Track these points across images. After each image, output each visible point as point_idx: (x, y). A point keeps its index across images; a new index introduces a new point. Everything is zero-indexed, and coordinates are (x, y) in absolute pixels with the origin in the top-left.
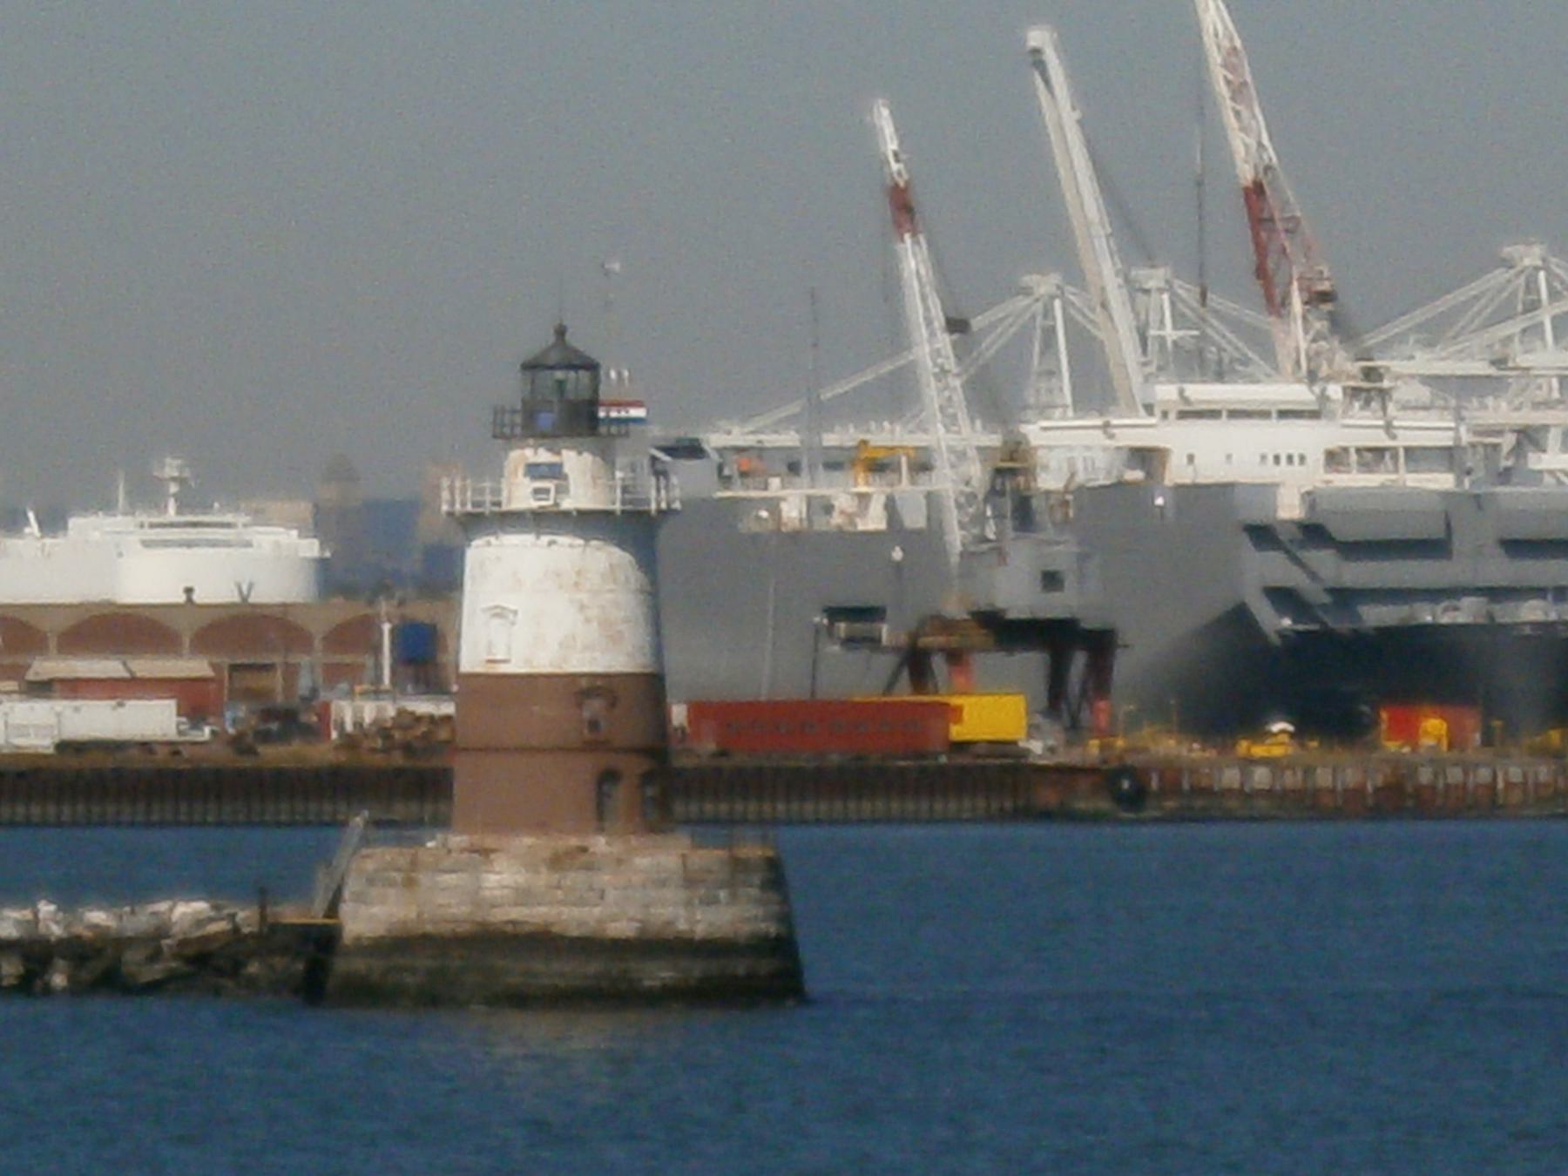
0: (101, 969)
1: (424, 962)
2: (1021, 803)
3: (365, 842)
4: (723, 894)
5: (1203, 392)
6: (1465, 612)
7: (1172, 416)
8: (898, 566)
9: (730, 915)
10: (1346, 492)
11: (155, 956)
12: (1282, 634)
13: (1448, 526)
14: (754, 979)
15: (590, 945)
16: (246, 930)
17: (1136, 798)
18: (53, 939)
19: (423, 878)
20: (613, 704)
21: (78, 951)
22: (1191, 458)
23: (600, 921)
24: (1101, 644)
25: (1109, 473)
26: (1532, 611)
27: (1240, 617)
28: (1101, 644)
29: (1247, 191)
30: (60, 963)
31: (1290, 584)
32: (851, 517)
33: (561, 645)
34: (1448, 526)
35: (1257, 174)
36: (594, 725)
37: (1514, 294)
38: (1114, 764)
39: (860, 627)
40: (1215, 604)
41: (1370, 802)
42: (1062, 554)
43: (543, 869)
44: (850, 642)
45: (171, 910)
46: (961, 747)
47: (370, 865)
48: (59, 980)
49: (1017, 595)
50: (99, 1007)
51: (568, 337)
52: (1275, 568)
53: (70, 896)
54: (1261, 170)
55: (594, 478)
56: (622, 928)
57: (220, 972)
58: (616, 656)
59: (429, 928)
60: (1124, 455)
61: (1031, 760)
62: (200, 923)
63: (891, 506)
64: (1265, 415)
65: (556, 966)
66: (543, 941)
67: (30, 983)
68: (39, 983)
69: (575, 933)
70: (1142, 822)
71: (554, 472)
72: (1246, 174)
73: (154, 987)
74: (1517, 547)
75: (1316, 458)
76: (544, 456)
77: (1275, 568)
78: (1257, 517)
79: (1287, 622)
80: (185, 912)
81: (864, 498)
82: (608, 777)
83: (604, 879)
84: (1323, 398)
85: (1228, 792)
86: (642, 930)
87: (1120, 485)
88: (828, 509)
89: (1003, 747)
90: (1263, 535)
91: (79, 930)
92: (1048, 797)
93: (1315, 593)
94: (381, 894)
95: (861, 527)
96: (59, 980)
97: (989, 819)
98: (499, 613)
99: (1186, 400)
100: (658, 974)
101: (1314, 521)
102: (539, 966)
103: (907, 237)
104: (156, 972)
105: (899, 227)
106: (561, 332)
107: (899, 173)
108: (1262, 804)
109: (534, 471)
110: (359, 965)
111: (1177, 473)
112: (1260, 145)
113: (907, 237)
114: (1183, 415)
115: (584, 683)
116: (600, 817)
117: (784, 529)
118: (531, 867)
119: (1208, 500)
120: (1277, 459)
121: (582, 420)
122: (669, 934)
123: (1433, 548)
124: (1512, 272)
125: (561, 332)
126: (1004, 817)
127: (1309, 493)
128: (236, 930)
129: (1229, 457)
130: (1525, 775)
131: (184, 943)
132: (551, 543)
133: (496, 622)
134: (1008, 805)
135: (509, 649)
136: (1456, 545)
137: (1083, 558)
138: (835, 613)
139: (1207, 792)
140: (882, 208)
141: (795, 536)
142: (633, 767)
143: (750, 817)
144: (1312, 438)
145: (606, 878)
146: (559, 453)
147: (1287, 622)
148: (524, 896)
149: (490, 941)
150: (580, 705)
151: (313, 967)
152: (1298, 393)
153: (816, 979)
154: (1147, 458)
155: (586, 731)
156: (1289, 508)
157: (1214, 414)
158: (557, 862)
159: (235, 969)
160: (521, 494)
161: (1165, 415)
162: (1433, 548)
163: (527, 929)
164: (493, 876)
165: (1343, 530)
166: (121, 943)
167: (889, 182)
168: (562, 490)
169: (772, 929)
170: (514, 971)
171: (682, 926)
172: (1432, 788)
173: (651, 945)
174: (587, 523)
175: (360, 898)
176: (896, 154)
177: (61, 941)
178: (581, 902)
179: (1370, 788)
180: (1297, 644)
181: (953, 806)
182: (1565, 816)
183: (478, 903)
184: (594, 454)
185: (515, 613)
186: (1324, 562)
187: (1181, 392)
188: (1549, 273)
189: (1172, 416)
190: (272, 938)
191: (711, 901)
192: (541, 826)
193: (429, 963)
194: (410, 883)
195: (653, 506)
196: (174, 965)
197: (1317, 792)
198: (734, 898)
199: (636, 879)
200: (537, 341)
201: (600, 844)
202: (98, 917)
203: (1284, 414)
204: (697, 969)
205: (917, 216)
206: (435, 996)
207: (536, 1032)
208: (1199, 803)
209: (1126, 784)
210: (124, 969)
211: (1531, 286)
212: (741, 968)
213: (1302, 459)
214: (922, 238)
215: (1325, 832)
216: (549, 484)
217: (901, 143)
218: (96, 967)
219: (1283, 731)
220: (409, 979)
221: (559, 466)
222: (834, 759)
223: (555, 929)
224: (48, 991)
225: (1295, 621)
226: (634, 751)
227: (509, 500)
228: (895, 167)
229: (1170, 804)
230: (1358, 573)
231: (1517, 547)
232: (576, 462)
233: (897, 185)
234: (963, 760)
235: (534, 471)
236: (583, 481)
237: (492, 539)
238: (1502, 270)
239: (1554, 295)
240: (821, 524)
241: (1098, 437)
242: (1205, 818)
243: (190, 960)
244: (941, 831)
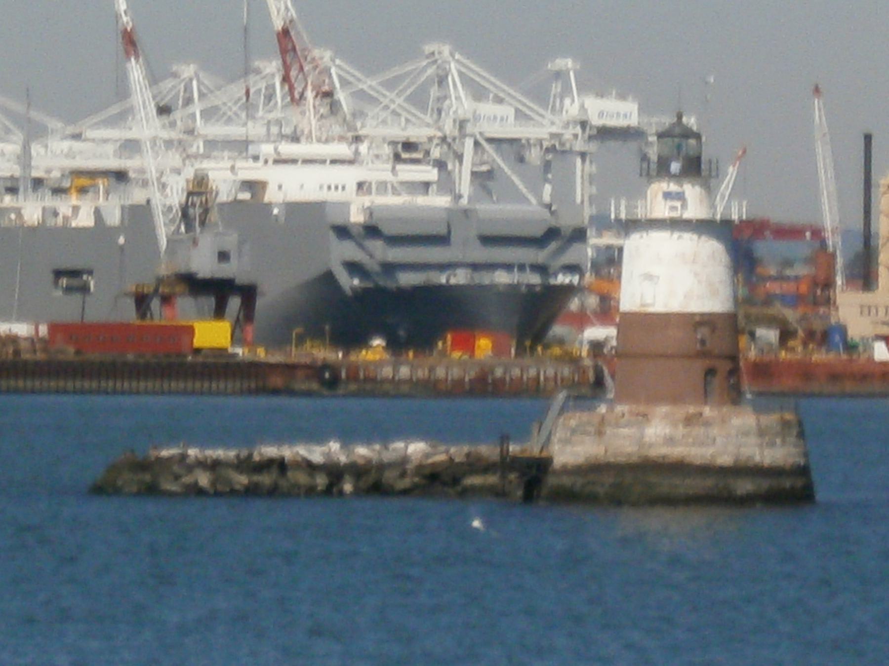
0: (373, 482)
1: (608, 480)
2: (261, 384)
3: (563, 410)
4: (778, 441)
5: (287, 149)
6: (460, 278)
7: (270, 162)
8: (122, 248)
9: (779, 454)
10: (387, 208)
11: (403, 475)
12: (353, 289)
13: (449, 226)
14: (788, 491)
15: (706, 470)
16: (457, 460)
17: (334, 383)
18: (342, 464)
19: (609, 431)
20: (713, 330)
21: (358, 471)
22: (280, 187)
23: (712, 456)
24: (248, 293)
25: (228, 196)
26: (502, 278)
27: (328, 277)
28: (248, 293)
29: (278, 34)
30: (347, 477)
31: (357, 259)
32: (66, 218)
33: (685, 297)
34: (449, 226)
35: (285, 23)
36: (703, 342)
37: (177, 94)
38: (319, 363)
39: (75, 282)
40: (314, 271)
41: (467, 387)
42: (230, 241)
43: (681, 427)
44: (68, 290)
45: (407, 447)
46: (198, 351)
47: (573, 423)
48: (348, 487)
49: (203, 263)
50: (369, 504)
52: (349, 251)
53: (348, 438)
54: (288, 22)
55: (701, 201)
56: (725, 460)
57: (445, 484)
59: (612, 460)
60: (238, 185)
61: (238, 359)
62: (427, 456)
63: (97, 213)
64: (323, 162)
65: (688, 481)
66: (680, 468)
67: (332, 490)
68: (335, 490)
69: (698, 463)
70: (334, 396)
71: (680, 197)
72: (278, 25)
73: (405, 492)
74: (488, 240)
75: (352, 187)
76: (673, 187)
77: (349, 251)
78: (339, 221)
79: (356, 282)
80: (416, 449)
81: (76, 209)
82: (710, 372)
83: (715, 431)
84: (357, 153)
85: (384, 381)
86: (736, 461)
87: (236, 202)
88: (56, 214)
89: (221, 352)
90: (343, 231)
91: (353, 458)
92: (277, 381)
93: (372, 265)
95: (74, 225)
96: (348, 487)
97: (241, 393)
98: (649, 277)
99: (278, 154)
100: (744, 487)
101: (373, 222)
102: (677, 481)
103: (133, 59)
104: (406, 483)
105: (128, 55)
107: (127, 23)
108: (405, 388)
109: (667, 195)
110: (566, 481)
111: (272, 195)
112: (287, 8)
113: (133, 59)
114: (277, 162)
115: (697, 319)
116: (706, 396)
117: (25, 225)
118: (675, 425)
119: (304, 213)
120: (329, 188)
121: (693, 168)
122: (751, 464)
123: (442, 240)
124: (178, 80)
126: (250, 392)
127: (369, 208)
128: (451, 460)
129: (302, 186)
130: (556, 373)
131: (420, 467)
132: (679, 237)
134: (253, 385)
136: (452, 239)
137: (241, 243)
138: (59, 274)
139: (374, 380)
140: (118, 44)
141: (33, 230)
142: (724, 366)
143: (109, 390)
144: (350, 176)
146: (682, 186)
147: (356, 282)
148: (670, 441)
150: (695, 331)
151: (533, 479)
152: (343, 150)
154: (255, 187)
155: (698, 345)
156: (356, 217)
157: (294, 161)
158: (689, 421)
159: (456, 481)
160: (661, 210)
161: (266, 162)
162: (442, 240)
163: (670, 461)
164: (655, 431)
165: (388, 229)
166: (382, 467)
167: (120, 27)
168: (684, 206)
169: (802, 462)
170: (665, 484)
171: (758, 459)
172: (502, 380)
173: (740, 470)
174: (702, 227)
175: (566, 442)
176: (125, 12)
177: (345, 465)
178: (702, 444)
179: (467, 379)
180: (361, 296)
181: (222, 385)
182: (883, 395)
183: (641, 444)
184: (701, 186)
185: (658, 277)
186: (377, 247)
187: (276, 149)
188: (198, 81)
189: (270, 162)
190: (507, 464)
191: (772, 444)
192: (676, 399)
194: (600, 433)
196: (416, 480)
197: (437, 382)
198: (784, 442)
199: (733, 432)
201: (707, 411)
202: (362, 451)
203: (334, 162)
204: (764, 484)
205: (138, 44)
206: (617, 499)
207: (655, 522)
208: (368, 387)
209: (327, 375)
210: (383, 480)
211: (188, 88)
212: (787, 483)
213: (344, 188)
214: (141, 60)
215: (446, 404)
216: (678, 204)
217: (128, 7)
218: (371, 479)
219: (378, 346)
221: (683, 193)
222: (130, 357)
223: (688, 460)
224: (341, 493)
225: (361, 281)
226: (714, 357)
227: (651, 213)
228: (125, 19)
229: (353, 387)
230: (396, 254)
231: (488, 240)
232: (692, 191)
233: (126, 29)
234: (200, 359)
235: (667, 195)
236: (694, 203)
237: (645, 235)
238: (171, 79)
239: (202, 95)
240: (51, 222)
241: (228, 174)
242: (372, 394)
243: (425, 477)
244: (193, 400)
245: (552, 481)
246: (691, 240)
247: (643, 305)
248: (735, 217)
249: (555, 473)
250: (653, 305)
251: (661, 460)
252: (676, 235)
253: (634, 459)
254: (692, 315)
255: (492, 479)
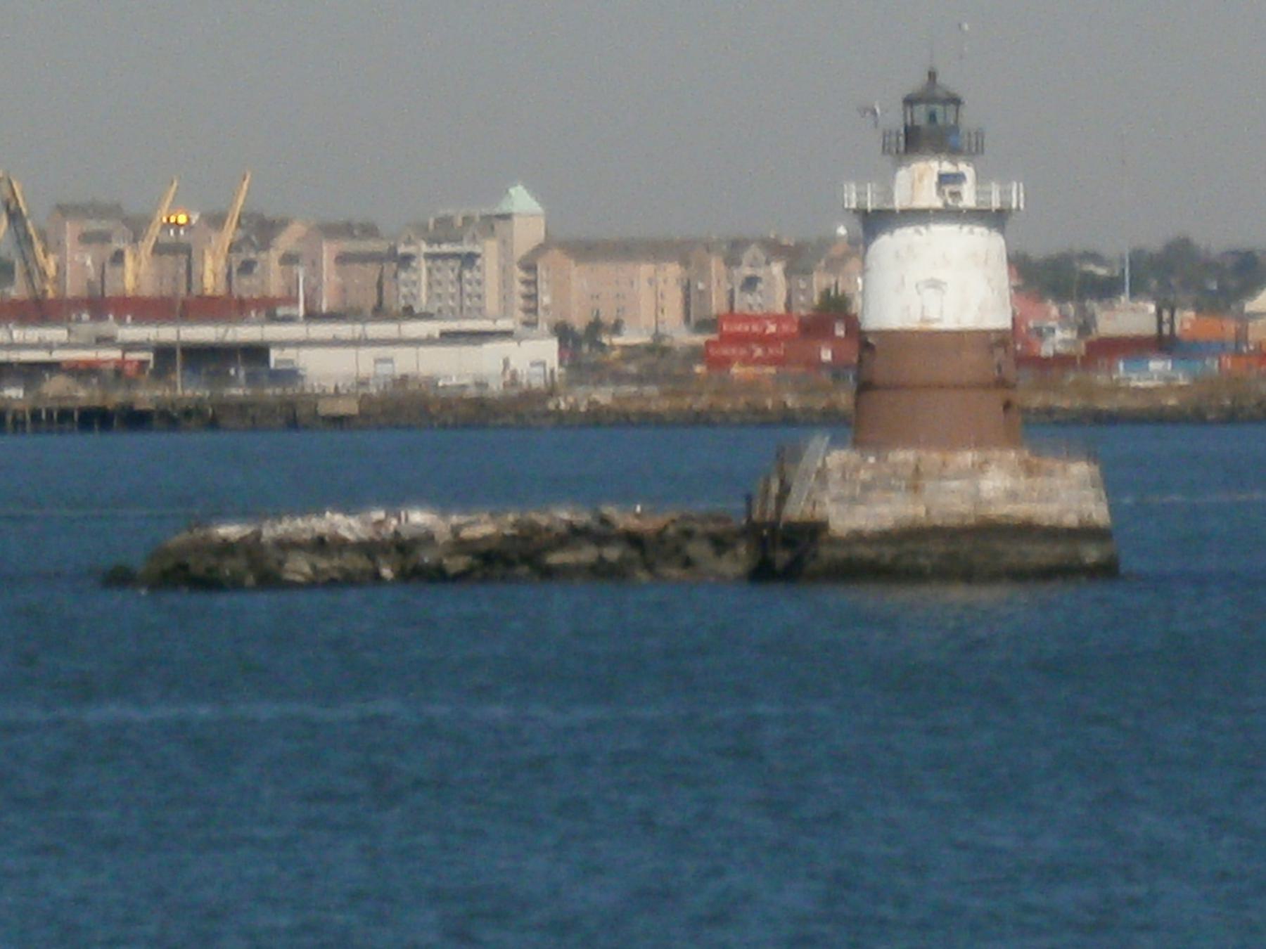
0: (410, 562)
1: (939, 547)
15: (1054, 533)
19: (929, 485)
51: (938, 79)
56: (1071, 520)
58: (999, 320)
59: (939, 522)
66: (1026, 530)
69: (1047, 523)
73: (461, 577)
76: (947, 167)
94: (853, 494)
98: (935, 284)
102: (1026, 548)
106: (932, 75)
115: (993, 338)
118: (1014, 475)
125: (932, 75)
133: (931, 291)
135: (942, 312)
145: (1058, 482)
148: (1013, 496)
149: (991, 531)
151: (788, 554)
153: (1123, 568)
160: (929, 197)
164: (991, 484)
183: (977, 499)
193: (942, 549)
194: (915, 488)
195: (1014, 205)
200: (915, 82)
220: (922, 561)
223: (1036, 521)
237: (922, 229)
245: (825, 552)
246: (982, 234)
247: (924, 320)
248: (870, 207)
249: (834, 541)
250: (938, 320)
251: (1004, 521)
252: (966, 229)
253: (971, 521)
254: (987, 333)
255: (587, 554)
